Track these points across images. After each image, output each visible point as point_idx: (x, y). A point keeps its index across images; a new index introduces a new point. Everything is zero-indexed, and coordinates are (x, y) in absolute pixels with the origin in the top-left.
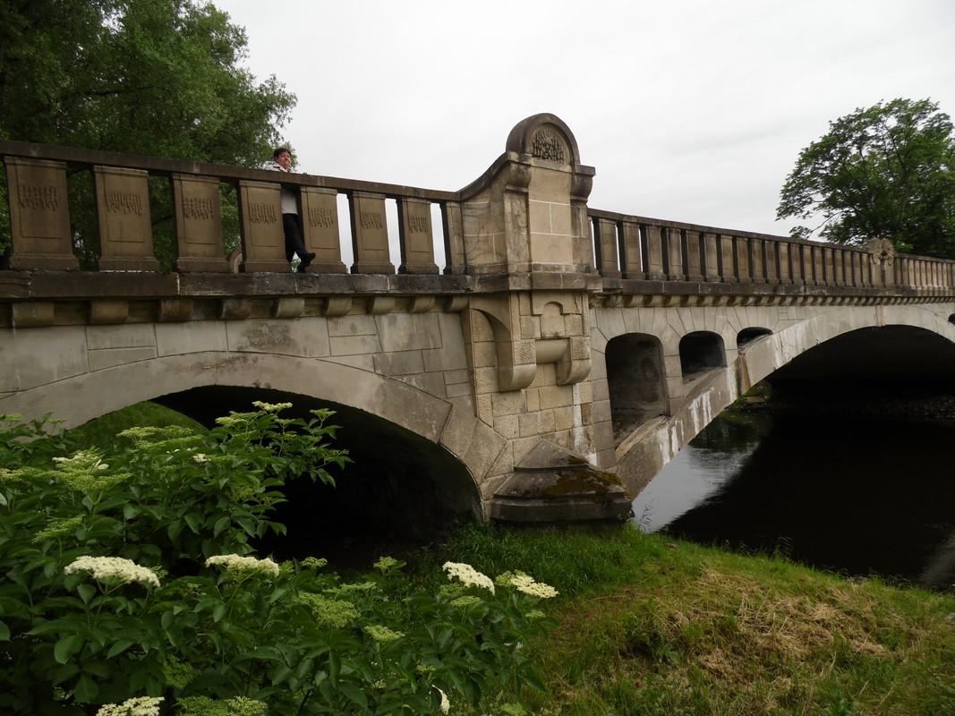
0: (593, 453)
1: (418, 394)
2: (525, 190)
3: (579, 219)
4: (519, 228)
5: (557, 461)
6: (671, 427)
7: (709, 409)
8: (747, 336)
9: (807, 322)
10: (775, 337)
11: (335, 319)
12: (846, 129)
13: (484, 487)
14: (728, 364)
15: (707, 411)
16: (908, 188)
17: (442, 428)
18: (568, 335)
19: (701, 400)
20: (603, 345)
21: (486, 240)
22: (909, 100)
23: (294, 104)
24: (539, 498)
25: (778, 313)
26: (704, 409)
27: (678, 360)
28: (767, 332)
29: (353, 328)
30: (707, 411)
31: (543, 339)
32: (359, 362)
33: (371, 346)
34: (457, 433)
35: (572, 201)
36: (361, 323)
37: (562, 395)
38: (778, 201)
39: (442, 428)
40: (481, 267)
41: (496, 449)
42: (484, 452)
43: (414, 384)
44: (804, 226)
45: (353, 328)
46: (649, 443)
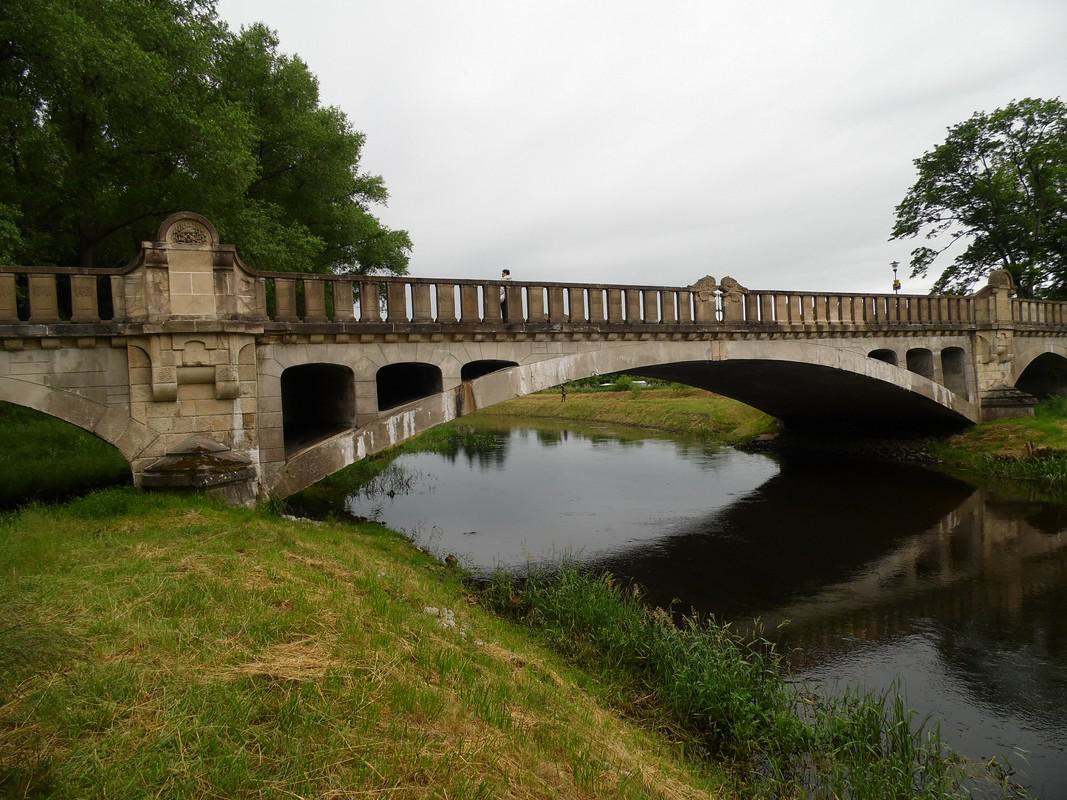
0: (255, 449)
1: (81, 400)
2: (165, 266)
3: (225, 282)
4: (161, 291)
5: (188, 449)
6: (358, 436)
7: (413, 425)
8: (472, 371)
9: (578, 356)
10: (521, 369)
11: (51, 351)
12: (967, 138)
13: (135, 464)
14: (445, 388)
15: (409, 426)
16: (1048, 195)
17: (96, 424)
18: (213, 363)
19: (402, 419)
20: (279, 372)
21: (140, 299)
22: (1040, 100)
23: (363, 142)
24: (159, 471)
25: (531, 348)
26: (405, 425)
27: (373, 389)
28: (514, 364)
29: (30, 357)
30: (409, 426)
31: (185, 366)
32: (32, 378)
33: (44, 368)
34: (110, 427)
35: (214, 270)
36: (38, 356)
37: (222, 407)
38: (893, 220)
39: (96, 424)
40: (136, 318)
41: (148, 441)
42: (136, 441)
43: (78, 393)
44: (927, 247)
45: (30, 357)
46: (328, 447)
